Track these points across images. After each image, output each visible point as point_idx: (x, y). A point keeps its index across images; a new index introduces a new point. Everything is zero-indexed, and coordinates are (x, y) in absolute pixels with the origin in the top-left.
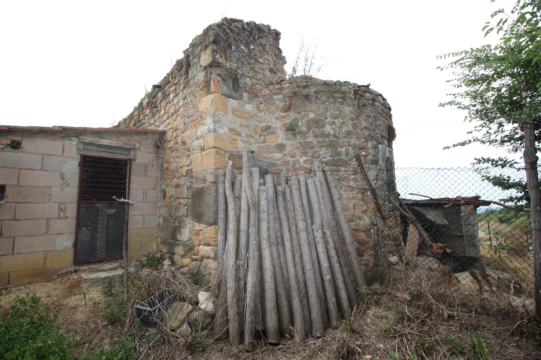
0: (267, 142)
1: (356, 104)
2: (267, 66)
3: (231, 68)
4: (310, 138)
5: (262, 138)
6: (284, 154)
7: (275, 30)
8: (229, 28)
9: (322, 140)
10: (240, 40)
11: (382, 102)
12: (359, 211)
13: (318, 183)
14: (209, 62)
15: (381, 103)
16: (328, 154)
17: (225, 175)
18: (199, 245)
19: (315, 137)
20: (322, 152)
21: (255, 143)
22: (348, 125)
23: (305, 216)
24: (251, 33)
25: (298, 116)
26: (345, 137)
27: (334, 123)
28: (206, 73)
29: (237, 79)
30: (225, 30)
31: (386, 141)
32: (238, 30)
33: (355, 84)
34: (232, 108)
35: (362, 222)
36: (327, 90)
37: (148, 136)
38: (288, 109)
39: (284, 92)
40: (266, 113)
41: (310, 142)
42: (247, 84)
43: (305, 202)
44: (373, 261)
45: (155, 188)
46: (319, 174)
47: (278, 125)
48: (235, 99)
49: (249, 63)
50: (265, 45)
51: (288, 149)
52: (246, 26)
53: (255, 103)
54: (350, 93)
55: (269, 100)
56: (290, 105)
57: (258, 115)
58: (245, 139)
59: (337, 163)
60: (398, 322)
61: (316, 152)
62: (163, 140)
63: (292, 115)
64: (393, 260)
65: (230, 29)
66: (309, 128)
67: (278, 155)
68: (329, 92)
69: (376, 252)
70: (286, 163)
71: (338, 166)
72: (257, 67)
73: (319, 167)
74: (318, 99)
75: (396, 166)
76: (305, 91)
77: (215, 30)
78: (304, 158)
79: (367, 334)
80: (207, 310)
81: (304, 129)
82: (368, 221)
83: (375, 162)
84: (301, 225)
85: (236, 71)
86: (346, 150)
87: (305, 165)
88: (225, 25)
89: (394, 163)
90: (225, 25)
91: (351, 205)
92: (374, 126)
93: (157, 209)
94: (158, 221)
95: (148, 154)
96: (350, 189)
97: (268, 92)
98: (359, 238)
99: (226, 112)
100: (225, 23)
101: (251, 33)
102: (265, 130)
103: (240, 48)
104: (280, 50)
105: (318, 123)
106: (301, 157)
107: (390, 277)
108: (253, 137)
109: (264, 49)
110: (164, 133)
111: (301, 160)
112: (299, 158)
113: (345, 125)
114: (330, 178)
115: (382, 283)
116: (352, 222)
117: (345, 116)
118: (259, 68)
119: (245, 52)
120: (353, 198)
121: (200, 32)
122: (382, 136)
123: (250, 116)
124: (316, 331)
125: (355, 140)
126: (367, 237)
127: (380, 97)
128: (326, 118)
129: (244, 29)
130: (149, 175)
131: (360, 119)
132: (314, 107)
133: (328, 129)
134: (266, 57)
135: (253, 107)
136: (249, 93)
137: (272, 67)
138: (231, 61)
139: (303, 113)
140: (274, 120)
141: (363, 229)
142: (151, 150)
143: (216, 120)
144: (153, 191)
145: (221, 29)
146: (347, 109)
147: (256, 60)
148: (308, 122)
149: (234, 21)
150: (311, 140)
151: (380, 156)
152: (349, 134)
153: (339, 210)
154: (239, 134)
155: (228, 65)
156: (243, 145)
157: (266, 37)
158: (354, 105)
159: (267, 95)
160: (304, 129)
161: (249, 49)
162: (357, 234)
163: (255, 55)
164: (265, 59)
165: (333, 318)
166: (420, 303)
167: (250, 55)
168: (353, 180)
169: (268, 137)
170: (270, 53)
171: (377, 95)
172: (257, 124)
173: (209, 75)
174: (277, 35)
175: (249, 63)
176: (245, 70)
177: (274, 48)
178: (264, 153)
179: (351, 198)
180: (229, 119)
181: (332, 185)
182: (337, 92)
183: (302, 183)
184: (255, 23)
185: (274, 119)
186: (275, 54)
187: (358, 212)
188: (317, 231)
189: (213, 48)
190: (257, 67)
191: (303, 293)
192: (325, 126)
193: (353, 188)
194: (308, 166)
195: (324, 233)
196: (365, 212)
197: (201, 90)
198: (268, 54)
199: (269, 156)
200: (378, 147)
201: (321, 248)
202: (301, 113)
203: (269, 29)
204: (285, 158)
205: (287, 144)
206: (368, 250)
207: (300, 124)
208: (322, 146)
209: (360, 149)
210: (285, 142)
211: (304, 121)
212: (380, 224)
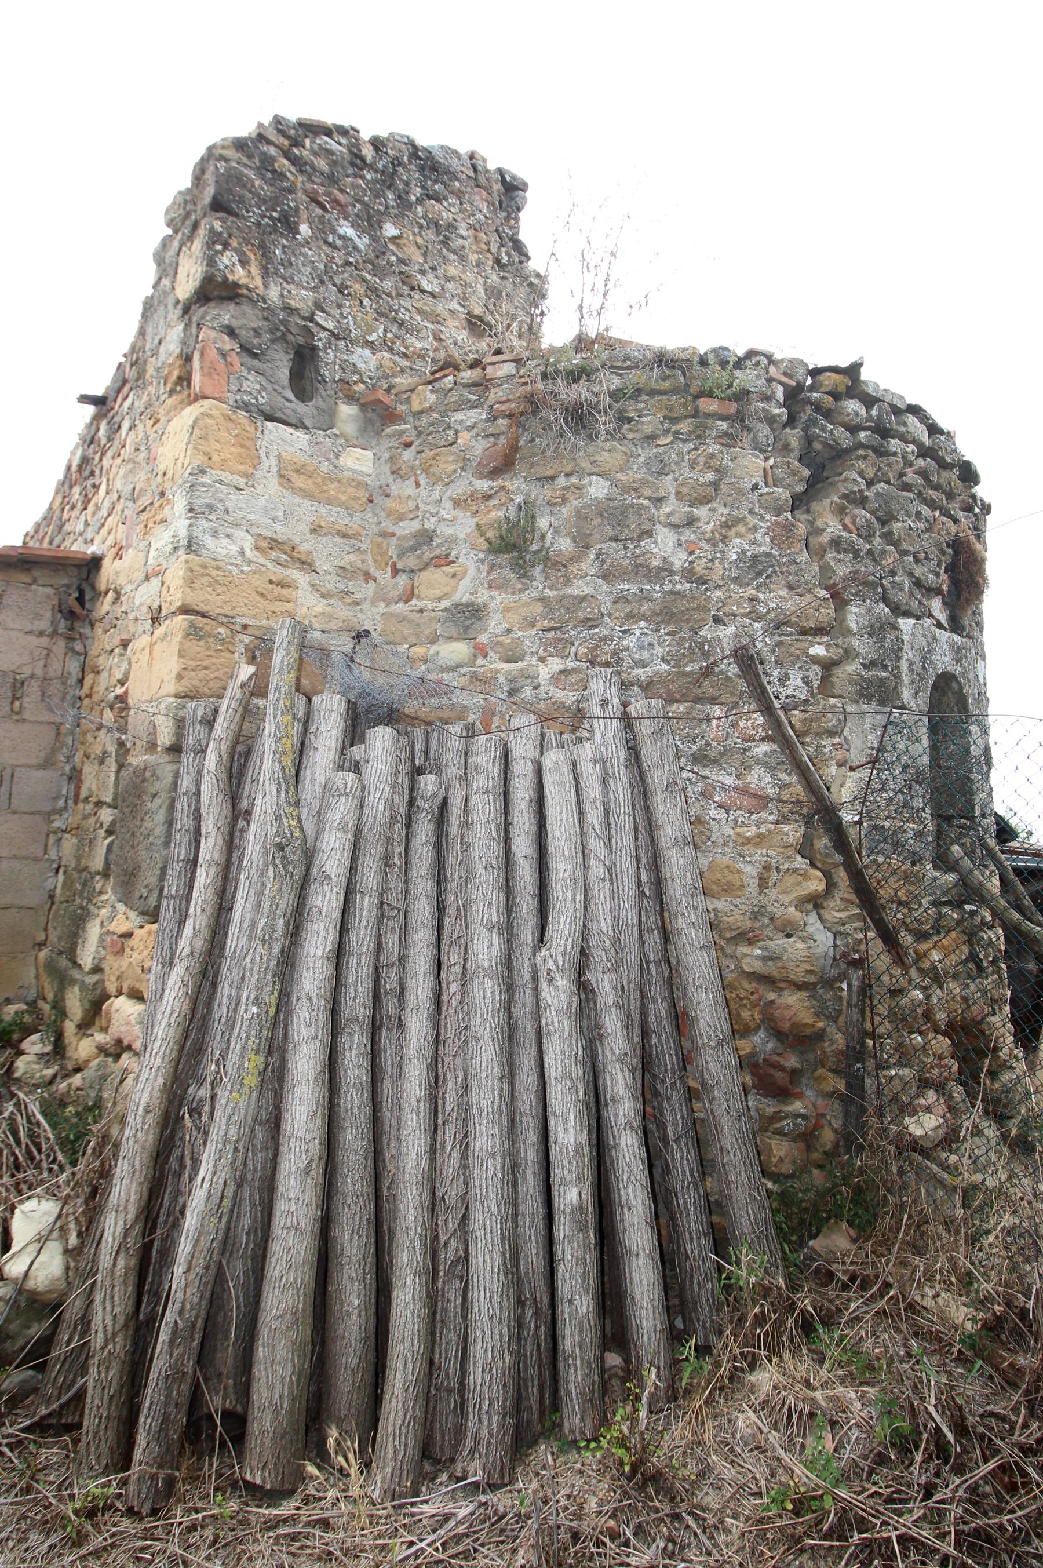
0: (419, 598)
1: (794, 443)
2: (454, 305)
3: (289, 309)
4: (585, 583)
5: (402, 579)
6: (476, 647)
7: (501, 172)
8: (287, 155)
9: (634, 588)
10: (336, 202)
11: (925, 438)
12: (786, 899)
13: (590, 772)
14: (197, 283)
15: (919, 445)
16: (658, 650)
17: (209, 723)
18: (120, 993)
19: (605, 576)
20: (631, 642)
21: (374, 603)
22: (755, 528)
23: (510, 908)
24: (388, 178)
25: (540, 493)
26: (736, 580)
27: (691, 522)
28: (187, 326)
29: (314, 349)
30: (267, 162)
31: (936, 606)
32: (334, 164)
33: (795, 363)
34: (279, 457)
35: (794, 949)
36: (666, 385)
37: (36, 573)
38: (504, 464)
39: (495, 394)
40: (423, 481)
41: (584, 598)
42: (355, 371)
43: (523, 846)
44: (837, 1124)
45: (48, 763)
46: (605, 732)
47: (459, 528)
48: (299, 425)
49: (373, 291)
50: (451, 226)
51: (495, 623)
52: (368, 152)
53: (385, 443)
54: (767, 398)
55: (433, 434)
56: (514, 448)
57: (395, 489)
58: (332, 583)
59: (689, 689)
60: (881, 1459)
61: (605, 639)
62: (93, 587)
63: (518, 486)
64: (918, 1132)
65: (295, 161)
66: (584, 544)
67: (455, 651)
68: (674, 391)
69: (856, 1085)
70: (482, 681)
71: (698, 700)
72: (407, 307)
73: (604, 703)
74: (630, 420)
75: (994, 709)
76: (581, 391)
77: (226, 160)
78: (555, 664)
79: (711, 1499)
80: (31, 1284)
81: (565, 545)
82: (824, 940)
83: (880, 692)
84: (486, 948)
85: (311, 319)
86: (737, 636)
87: (558, 694)
88: (269, 142)
89: (981, 698)
90: (269, 142)
91: (750, 871)
92: (877, 541)
93: (52, 839)
94: (49, 884)
95: (29, 638)
96: (746, 801)
97: (432, 398)
98: (777, 1013)
99: (247, 476)
100: (272, 135)
101: (388, 178)
102: (413, 549)
103: (334, 232)
104: (518, 246)
105: (624, 521)
106: (542, 660)
107: (902, 1207)
108: (368, 577)
109: (445, 242)
110: (95, 563)
111: (544, 673)
112: (534, 660)
113: (741, 529)
114: (649, 751)
115: (863, 1230)
116: (751, 942)
117: (741, 493)
118: (419, 311)
119: (356, 248)
120: (760, 839)
121: (186, 182)
122: (918, 583)
123: (363, 495)
124: (472, 1451)
125: (784, 592)
126: (817, 1015)
127: (911, 419)
128: (659, 501)
129: (357, 161)
130: (26, 715)
131: (815, 506)
132: (608, 453)
133: (664, 546)
134: (452, 270)
135: (377, 458)
136: (363, 407)
137: (478, 311)
138: (289, 280)
139: (562, 481)
140: (447, 511)
141: (801, 978)
142: (44, 624)
143: (200, 501)
144: (40, 773)
145: (250, 157)
146: (750, 466)
147: (405, 278)
148: (581, 515)
149: (312, 129)
150: (587, 590)
151: (904, 665)
152: (756, 567)
153: (676, 889)
154: (306, 564)
155: (273, 294)
156: (320, 606)
157: (459, 195)
158: (786, 448)
159: (431, 409)
160: (565, 545)
161: (374, 239)
162: (772, 996)
163: (401, 261)
164: (448, 279)
165: (568, 1393)
166: (1021, 1361)
167: (377, 260)
168: (766, 765)
169: (423, 575)
170: (473, 258)
171: (896, 411)
172: (388, 525)
173: (194, 330)
174: (510, 191)
175: (373, 291)
176: (353, 316)
177: (494, 238)
178: (405, 639)
179: (748, 841)
180: (265, 504)
181: (657, 778)
182: (710, 395)
183: (521, 768)
184: (412, 144)
185: (449, 505)
186: (498, 261)
187: (782, 901)
188: (550, 981)
189: (212, 230)
190: (407, 307)
191: (451, 1255)
192: (649, 533)
193: (762, 801)
194: (569, 697)
195: (583, 988)
196: (815, 902)
197: (172, 392)
198: (463, 259)
199: (419, 651)
200: (895, 628)
201: (561, 1055)
202: (553, 478)
203: (474, 167)
204: (480, 661)
205: (492, 605)
206: (821, 1071)
207: (543, 523)
208: (631, 617)
209: (804, 632)
210: (483, 596)
211: (565, 510)
212: (880, 959)
